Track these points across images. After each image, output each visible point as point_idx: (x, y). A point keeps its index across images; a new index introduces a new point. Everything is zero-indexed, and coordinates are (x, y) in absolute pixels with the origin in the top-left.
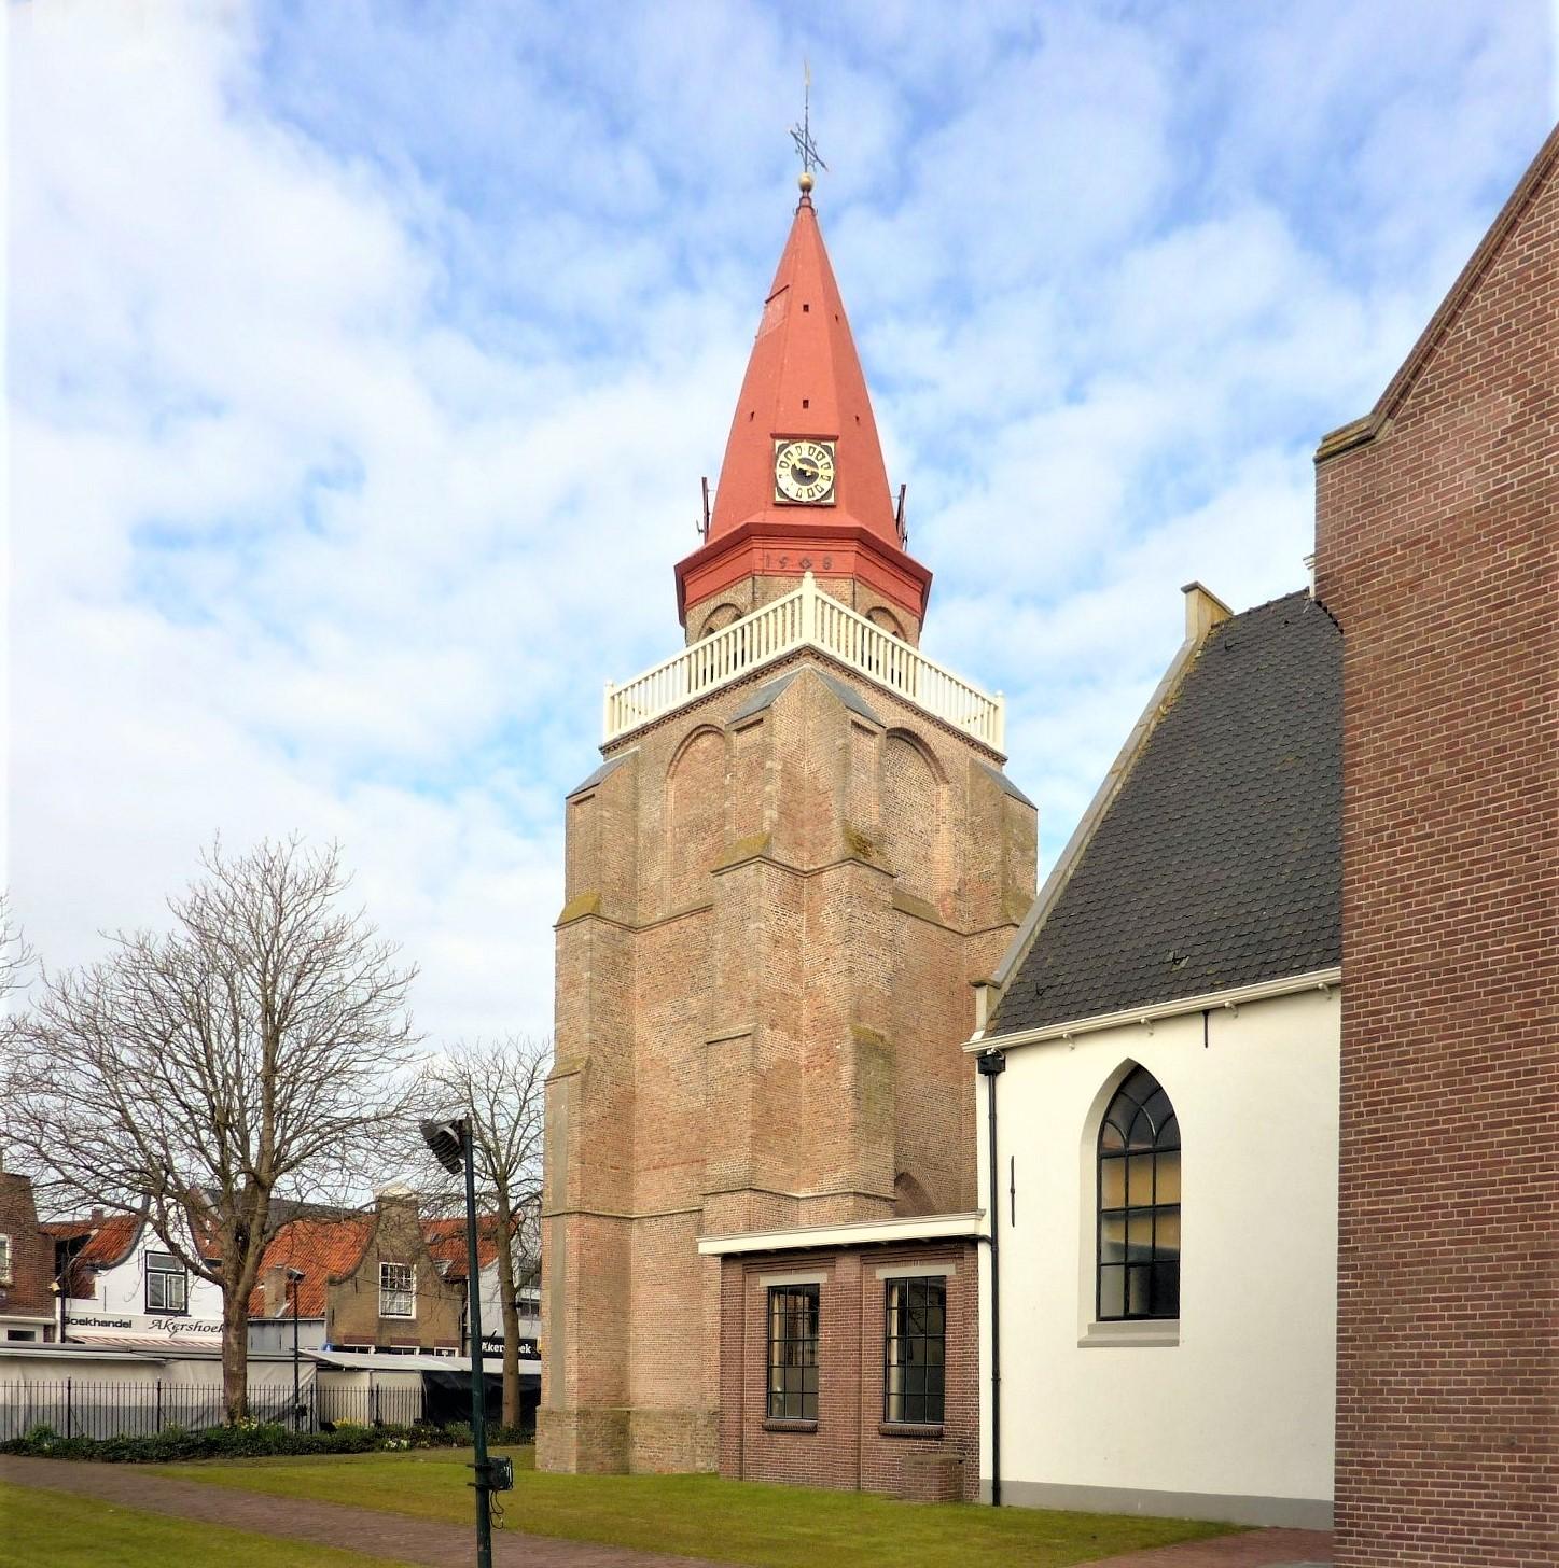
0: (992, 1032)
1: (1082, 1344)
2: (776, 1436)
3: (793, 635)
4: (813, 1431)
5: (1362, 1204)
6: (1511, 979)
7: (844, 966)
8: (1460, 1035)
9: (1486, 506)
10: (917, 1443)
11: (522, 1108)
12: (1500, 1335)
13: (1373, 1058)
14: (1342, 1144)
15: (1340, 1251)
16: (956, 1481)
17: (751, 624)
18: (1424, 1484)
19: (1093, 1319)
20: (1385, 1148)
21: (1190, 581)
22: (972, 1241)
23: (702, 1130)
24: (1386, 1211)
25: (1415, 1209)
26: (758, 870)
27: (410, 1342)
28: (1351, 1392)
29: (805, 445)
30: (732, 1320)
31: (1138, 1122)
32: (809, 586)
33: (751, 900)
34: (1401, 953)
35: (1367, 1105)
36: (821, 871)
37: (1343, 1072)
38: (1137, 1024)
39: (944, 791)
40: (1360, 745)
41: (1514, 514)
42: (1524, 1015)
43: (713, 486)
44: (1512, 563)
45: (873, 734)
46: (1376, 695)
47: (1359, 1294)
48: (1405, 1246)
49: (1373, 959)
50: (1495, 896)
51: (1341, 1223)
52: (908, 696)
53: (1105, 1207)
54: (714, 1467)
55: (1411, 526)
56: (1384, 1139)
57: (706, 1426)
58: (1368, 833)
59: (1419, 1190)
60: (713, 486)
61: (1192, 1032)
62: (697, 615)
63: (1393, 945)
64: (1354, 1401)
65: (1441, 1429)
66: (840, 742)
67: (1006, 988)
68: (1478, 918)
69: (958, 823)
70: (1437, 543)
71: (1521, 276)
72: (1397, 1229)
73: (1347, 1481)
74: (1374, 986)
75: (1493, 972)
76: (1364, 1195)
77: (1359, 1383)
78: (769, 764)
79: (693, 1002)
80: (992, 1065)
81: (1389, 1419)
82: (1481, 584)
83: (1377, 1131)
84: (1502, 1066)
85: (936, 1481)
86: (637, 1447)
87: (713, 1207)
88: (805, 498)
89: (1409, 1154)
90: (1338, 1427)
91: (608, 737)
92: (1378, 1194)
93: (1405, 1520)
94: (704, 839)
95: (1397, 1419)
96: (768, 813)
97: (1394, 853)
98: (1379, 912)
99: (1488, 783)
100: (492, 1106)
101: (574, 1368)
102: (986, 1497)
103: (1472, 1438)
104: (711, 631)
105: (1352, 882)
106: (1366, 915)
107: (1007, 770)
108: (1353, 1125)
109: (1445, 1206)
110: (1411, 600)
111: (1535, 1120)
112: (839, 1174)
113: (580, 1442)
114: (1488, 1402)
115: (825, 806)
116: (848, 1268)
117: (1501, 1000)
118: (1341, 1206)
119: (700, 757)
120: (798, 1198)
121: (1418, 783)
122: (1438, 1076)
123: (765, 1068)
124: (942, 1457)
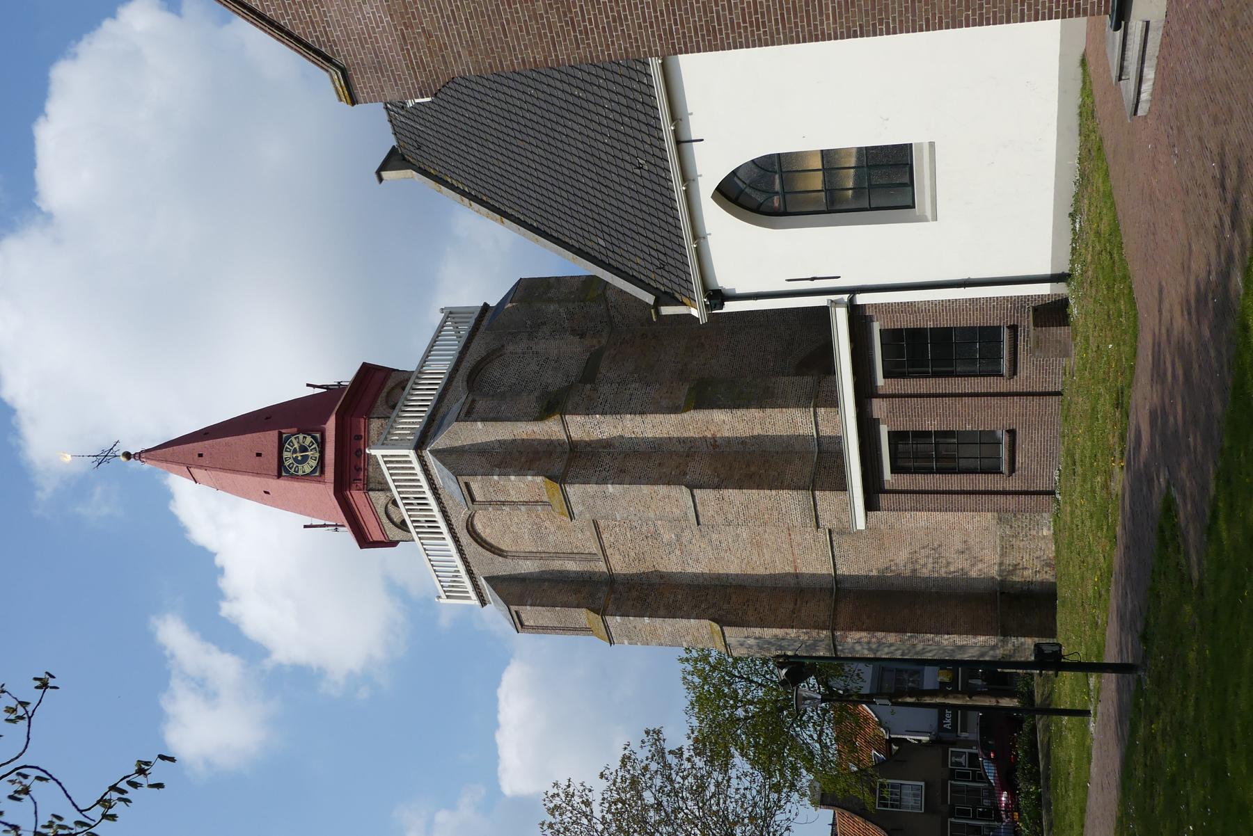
3: (406, 462)
5: (828, 25)
10: (1020, 347)
13: (726, 29)
14: (786, 43)
15: (862, 36)
20: (789, 13)
21: (375, 177)
24: (834, 8)
28: (968, 16)
29: (285, 454)
31: (765, 191)
34: (656, 17)
35: (758, 29)
37: (735, 48)
39: (510, 348)
43: (309, 521)
46: (493, 52)
51: (842, 38)
54: (1047, 517)
56: (782, 15)
58: (578, 48)
62: (394, 533)
63: (651, 24)
69: (531, 337)
74: (678, 33)
76: (822, 24)
79: (666, 538)
80: (717, 297)
83: (776, 20)
87: (827, 520)
91: (477, 603)
92: (821, 13)
97: (592, 30)
102: (1061, 289)
104: (403, 522)
105: (609, 55)
106: (631, 44)
107: (493, 303)
108: (772, 37)
112: (799, 420)
116: (879, 408)
118: (830, 39)
121: (548, 18)
124: (1032, 327)
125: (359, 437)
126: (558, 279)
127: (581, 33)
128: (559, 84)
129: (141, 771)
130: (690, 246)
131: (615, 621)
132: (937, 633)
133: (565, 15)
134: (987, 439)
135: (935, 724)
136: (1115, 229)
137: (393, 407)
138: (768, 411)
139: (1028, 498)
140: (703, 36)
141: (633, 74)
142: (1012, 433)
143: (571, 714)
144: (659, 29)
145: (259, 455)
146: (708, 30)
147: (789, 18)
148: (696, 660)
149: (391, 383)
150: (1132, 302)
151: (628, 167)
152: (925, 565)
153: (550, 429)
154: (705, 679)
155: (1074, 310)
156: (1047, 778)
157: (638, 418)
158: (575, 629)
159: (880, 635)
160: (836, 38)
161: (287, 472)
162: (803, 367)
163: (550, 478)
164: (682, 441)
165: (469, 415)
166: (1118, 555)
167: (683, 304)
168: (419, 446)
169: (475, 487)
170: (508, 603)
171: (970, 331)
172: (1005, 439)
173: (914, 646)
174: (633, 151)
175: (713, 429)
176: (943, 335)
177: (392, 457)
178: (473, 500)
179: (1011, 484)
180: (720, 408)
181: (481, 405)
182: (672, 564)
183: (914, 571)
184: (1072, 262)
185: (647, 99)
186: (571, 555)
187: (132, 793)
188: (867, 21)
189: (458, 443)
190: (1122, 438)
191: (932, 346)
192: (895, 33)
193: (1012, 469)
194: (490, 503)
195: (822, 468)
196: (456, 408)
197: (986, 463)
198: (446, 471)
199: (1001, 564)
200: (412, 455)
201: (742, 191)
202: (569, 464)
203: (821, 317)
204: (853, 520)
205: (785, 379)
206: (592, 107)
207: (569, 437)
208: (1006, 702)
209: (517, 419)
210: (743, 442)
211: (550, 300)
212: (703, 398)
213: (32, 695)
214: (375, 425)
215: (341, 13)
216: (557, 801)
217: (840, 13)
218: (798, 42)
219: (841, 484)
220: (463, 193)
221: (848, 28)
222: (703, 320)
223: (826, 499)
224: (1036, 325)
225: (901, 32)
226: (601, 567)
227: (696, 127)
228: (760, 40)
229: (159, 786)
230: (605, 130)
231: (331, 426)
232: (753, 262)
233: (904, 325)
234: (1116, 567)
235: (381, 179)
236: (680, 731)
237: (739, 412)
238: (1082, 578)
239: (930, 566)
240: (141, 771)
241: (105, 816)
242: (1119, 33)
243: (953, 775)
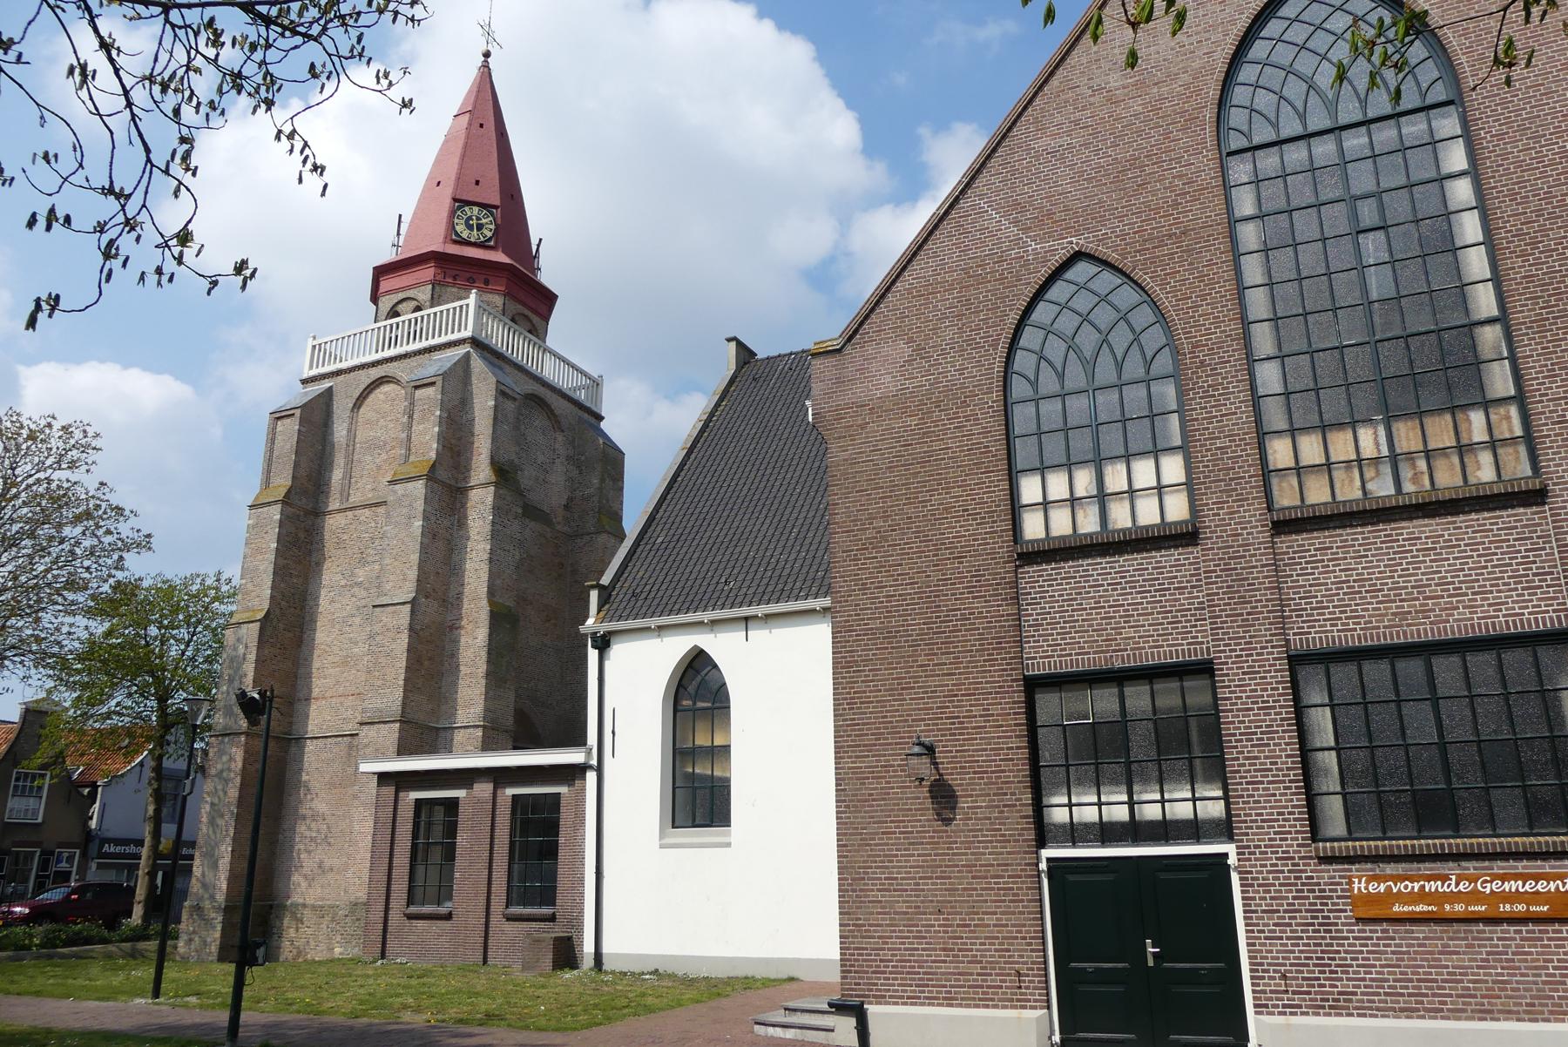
2: (414, 922)
21: (731, 335)
29: (476, 209)
31: (697, 693)
39: (560, 437)
43: (406, 220)
54: (355, 951)
60: (406, 220)
62: (386, 303)
69: (568, 458)
71: (909, 291)
91: (305, 376)
102: (588, 962)
104: (397, 314)
107: (603, 425)
116: (483, 789)
125: (487, 282)
126: (621, 489)
128: (803, 515)
129: (315, 168)
130: (653, 622)
131: (275, 513)
132: (234, 840)
134: (444, 892)
135: (110, 835)
136: (650, 1010)
137: (513, 320)
138: (483, 682)
139: (380, 932)
141: (808, 583)
142: (448, 917)
143: (163, 448)
145: (477, 183)
148: (217, 589)
149: (535, 319)
150: (588, 1026)
151: (728, 571)
152: (309, 829)
153: (481, 470)
154: (194, 596)
155: (568, 975)
156: (50, 957)
157: (486, 556)
158: (269, 472)
159: (238, 780)
162: (521, 716)
163: (433, 465)
164: (459, 597)
165: (502, 393)
166: (338, 1019)
167: (599, 611)
168: (475, 342)
169: (430, 391)
170: (303, 407)
171: (553, 876)
172: (442, 910)
173: (222, 816)
174: (740, 578)
175: (470, 627)
176: (550, 851)
177: (466, 314)
178: (416, 387)
179: (395, 916)
180: (490, 635)
181: (510, 406)
182: (331, 575)
183: (304, 818)
184: (613, 972)
185: (785, 594)
186: (348, 475)
187: (297, 157)
189: (474, 380)
190: (460, 1021)
191: (540, 843)
193: (410, 917)
194: (412, 404)
195: (421, 731)
196: (508, 381)
197: (419, 892)
198: (448, 365)
199: (304, 906)
200: (468, 333)
201: (698, 672)
202: (446, 485)
203: (575, 738)
204: (366, 759)
205: (512, 698)
206: (781, 544)
207: (472, 488)
208: (138, 911)
209: (494, 439)
210: (454, 655)
211: (602, 480)
212: (500, 619)
213: (397, 93)
214: (498, 300)
216: (78, 434)
219: (403, 750)
220: (712, 414)
222: (582, 629)
223: (391, 733)
224: (556, 939)
226: (334, 504)
227: (759, 635)
229: (300, 181)
230: (761, 553)
231: (499, 257)
232: (631, 680)
233: (563, 816)
234: (326, 1019)
235: (729, 340)
236: (141, 568)
237: (484, 654)
238: (302, 987)
239: (308, 833)
240: (315, 168)
241: (280, 132)
242: (825, 1007)
243: (47, 855)
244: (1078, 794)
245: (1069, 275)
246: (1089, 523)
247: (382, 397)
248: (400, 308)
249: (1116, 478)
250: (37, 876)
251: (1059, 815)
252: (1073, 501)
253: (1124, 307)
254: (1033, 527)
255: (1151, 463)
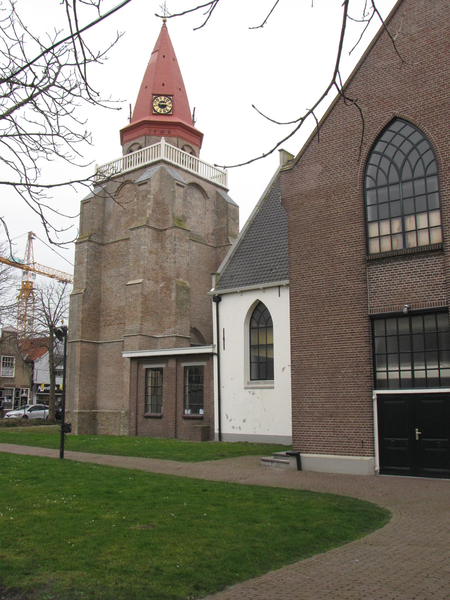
0: (217, 289)
1: (246, 388)
3: (157, 156)
4: (161, 417)
6: (326, 300)
7: (173, 261)
8: (316, 312)
9: (316, 189)
10: (195, 421)
11: (60, 301)
12: (327, 388)
14: (291, 338)
16: (207, 433)
17: (144, 151)
18: (312, 426)
19: (249, 379)
22: (211, 355)
23: (124, 313)
25: (307, 355)
26: (145, 230)
27: (11, 386)
29: (163, 98)
30: (135, 379)
32: (163, 141)
33: (142, 239)
34: (302, 291)
35: (296, 328)
36: (166, 230)
37: (290, 320)
38: (259, 289)
40: (292, 240)
41: (322, 192)
42: (329, 309)
44: (322, 203)
45: (183, 187)
47: (296, 377)
48: (306, 365)
49: (296, 292)
50: (322, 279)
52: (196, 173)
53: (252, 344)
55: (301, 190)
57: (124, 417)
59: (309, 350)
61: (275, 293)
64: (296, 405)
65: (315, 412)
66: (172, 190)
67: (222, 274)
68: (318, 284)
70: (306, 195)
72: (304, 360)
73: (295, 426)
75: (322, 298)
76: (297, 351)
77: (297, 400)
78: (149, 196)
80: (218, 299)
81: (304, 410)
82: (316, 206)
83: (298, 335)
84: (325, 321)
85: (200, 433)
86: (99, 425)
88: (162, 112)
89: (306, 341)
90: (292, 412)
93: (308, 436)
94: (127, 216)
95: (306, 409)
96: (148, 211)
98: (297, 281)
99: (319, 252)
100: (49, 300)
101: (78, 396)
102: (217, 438)
103: (322, 414)
104: (131, 151)
106: (294, 281)
107: (229, 193)
108: (293, 333)
109: (314, 355)
110: (301, 207)
111: (333, 334)
113: (79, 423)
114: (326, 405)
115: (167, 209)
116: (172, 364)
117: (324, 304)
118: (291, 354)
119: (126, 190)
120: (157, 337)
121: (305, 250)
122: (312, 322)
123: (145, 293)
127: (299, 262)
130: (239, 289)
133: (306, 257)
140: (295, 308)
144: (299, 292)
145: (163, 85)
146: (297, 310)
147: (299, 340)
149: (194, 147)
160: (291, 356)
161: (155, 98)
179: (140, 419)
188: (296, 368)
192: (292, 377)
215: (312, 171)
217: (299, 358)
218: (291, 343)
221: (294, 361)
225: (292, 379)
228: (293, 329)
233: (205, 375)
244: (429, 365)
245: (391, 128)
246: (398, 245)
247: (126, 190)
248: (133, 148)
249: (410, 224)
250: (15, 399)
251: (381, 376)
252: (391, 235)
253: (415, 142)
254: (374, 248)
255: (413, 218)
